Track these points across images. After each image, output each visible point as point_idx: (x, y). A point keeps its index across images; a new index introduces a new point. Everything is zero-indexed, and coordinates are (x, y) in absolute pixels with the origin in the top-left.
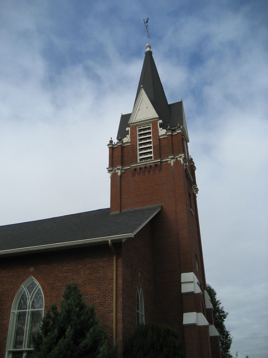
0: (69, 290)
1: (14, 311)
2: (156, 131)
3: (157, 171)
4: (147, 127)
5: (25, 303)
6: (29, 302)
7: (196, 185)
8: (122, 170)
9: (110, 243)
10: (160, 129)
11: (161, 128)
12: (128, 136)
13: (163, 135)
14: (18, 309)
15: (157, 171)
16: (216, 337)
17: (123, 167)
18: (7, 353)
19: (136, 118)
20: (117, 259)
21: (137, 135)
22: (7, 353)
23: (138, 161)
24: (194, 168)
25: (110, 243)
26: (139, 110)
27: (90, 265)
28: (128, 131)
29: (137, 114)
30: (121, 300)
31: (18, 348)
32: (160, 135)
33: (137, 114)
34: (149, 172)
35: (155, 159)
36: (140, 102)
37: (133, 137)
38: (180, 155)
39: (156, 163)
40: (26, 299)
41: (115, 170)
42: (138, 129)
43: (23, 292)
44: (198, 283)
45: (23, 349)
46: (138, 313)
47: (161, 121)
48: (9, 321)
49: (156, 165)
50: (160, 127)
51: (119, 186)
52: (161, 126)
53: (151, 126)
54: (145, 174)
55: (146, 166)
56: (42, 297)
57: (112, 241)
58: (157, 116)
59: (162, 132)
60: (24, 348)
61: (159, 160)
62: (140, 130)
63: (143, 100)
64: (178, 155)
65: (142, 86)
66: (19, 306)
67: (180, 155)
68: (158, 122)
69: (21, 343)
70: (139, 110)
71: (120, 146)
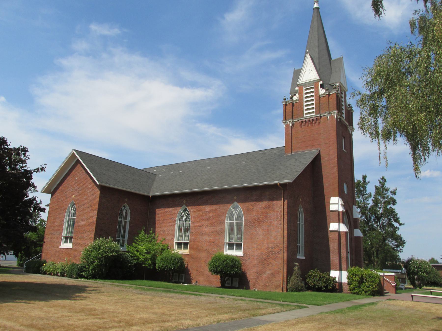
0: (196, 308)
1: (227, 221)
2: (317, 91)
3: (317, 124)
4: (311, 87)
5: (233, 217)
6: (235, 217)
7: (352, 127)
8: (292, 121)
9: (278, 184)
10: (320, 89)
11: (322, 88)
12: (297, 95)
13: (322, 94)
14: (229, 221)
15: (317, 124)
16: (359, 238)
17: (293, 120)
18: (225, 243)
19: (302, 79)
20: (284, 191)
21: (304, 93)
22: (225, 243)
23: (304, 116)
24: (351, 111)
25: (278, 184)
26: (305, 72)
27: (269, 197)
28: (297, 90)
29: (303, 76)
30: (286, 218)
31: (231, 241)
32: (320, 94)
33: (303, 76)
34: (312, 124)
35: (316, 114)
36: (306, 65)
37: (301, 96)
38: (334, 112)
39: (317, 117)
40: (233, 214)
41: (288, 122)
42: (304, 88)
43: (231, 211)
44: (341, 204)
45: (234, 242)
46: (299, 224)
47: (321, 82)
48: (225, 227)
49: (317, 119)
50: (321, 87)
51: (291, 134)
52: (322, 86)
53: (314, 86)
54: (309, 125)
55: (309, 119)
56: (242, 214)
57: (233, 249)
58: (318, 78)
59: (322, 91)
60: (234, 241)
61: (319, 115)
62: (306, 90)
63: (308, 64)
64: (333, 112)
65: (307, 51)
66: (229, 219)
67: (334, 112)
68: (320, 83)
69: (232, 239)
70: (305, 72)
71: (291, 103)
